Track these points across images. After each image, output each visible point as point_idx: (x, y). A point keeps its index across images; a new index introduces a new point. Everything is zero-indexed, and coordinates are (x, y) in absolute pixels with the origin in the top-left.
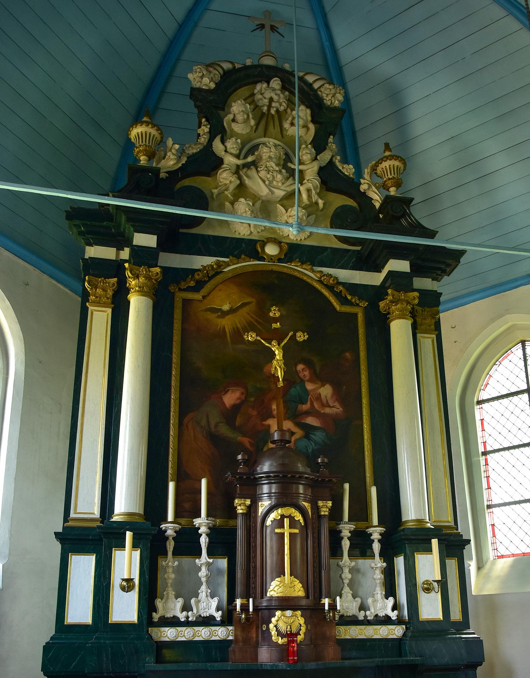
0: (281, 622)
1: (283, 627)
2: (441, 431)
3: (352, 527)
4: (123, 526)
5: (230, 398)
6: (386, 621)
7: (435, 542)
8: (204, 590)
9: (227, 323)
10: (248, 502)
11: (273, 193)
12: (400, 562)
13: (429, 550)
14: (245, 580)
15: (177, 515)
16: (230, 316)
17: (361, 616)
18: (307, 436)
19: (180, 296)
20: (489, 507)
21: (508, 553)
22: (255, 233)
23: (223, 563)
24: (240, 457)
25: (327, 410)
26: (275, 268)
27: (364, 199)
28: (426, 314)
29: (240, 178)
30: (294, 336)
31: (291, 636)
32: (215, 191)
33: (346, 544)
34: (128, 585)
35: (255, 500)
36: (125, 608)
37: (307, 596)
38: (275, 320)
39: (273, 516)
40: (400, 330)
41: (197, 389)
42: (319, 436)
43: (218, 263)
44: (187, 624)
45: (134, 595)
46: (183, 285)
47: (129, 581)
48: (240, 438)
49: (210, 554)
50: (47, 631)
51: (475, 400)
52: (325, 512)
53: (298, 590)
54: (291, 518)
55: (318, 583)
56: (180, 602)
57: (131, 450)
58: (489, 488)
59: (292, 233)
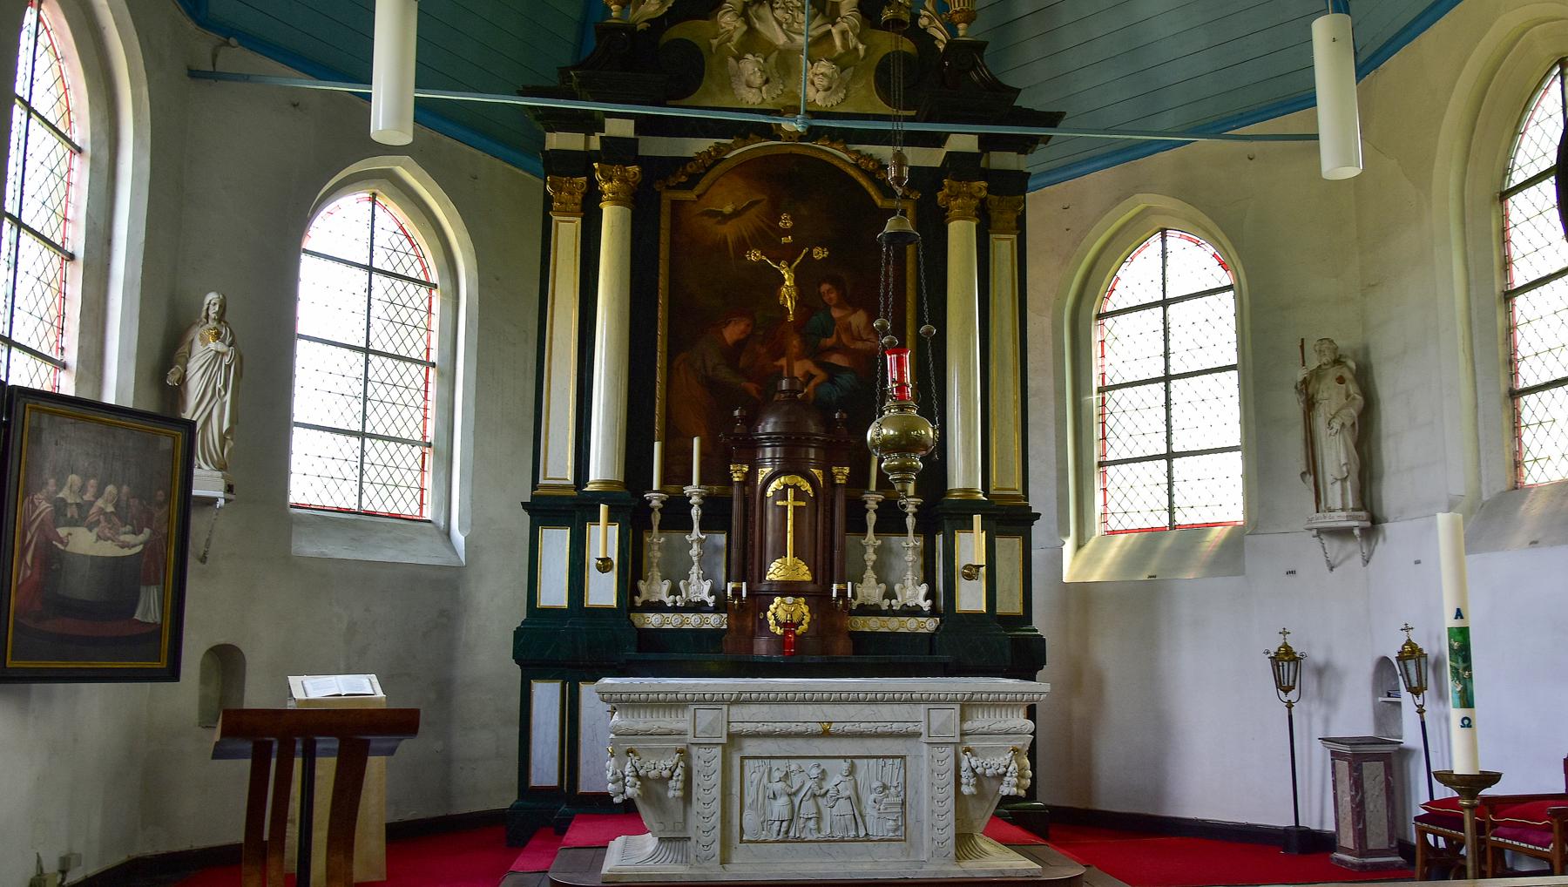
0: (779, 609)
1: (782, 615)
2: (1015, 369)
3: (880, 497)
4: (597, 497)
5: (732, 333)
6: (915, 612)
7: (977, 519)
8: (695, 571)
9: (729, 231)
10: (746, 469)
11: (791, 40)
12: (939, 539)
13: (971, 528)
14: (747, 563)
15: (665, 480)
16: (734, 222)
17: (885, 605)
18: (831, 380)
19: (667, 197)
20: (1101, 464)
21: (1120, 528)
22: (769, 100)
23: (721, 539)
24: (737, 413)
25: (859, 345)
26: (795, 150)
27: (923, 38)
28: (1002, 201)
29: (748, 22)
30: (810, 253)
31: (789, 626)
32: (715, 42)
33: (872, 518)
34: (605, 565)
35: (754, 467)
36: (603, 591)
37: (815, 580)
38: (786, 232)
39: (775, 485)
40: (960, 235)
41: (691, 323)
42: (846, 380)
43: (718, 147)
44: (675, 609)
45: (612, 577)
46: (672, 182)
47: (606, 560)
48: (745, 384)
49: (703, 529)
50: (519, 615)
51: (1094, 313)
52: (840, 480)
53: (804, 573)
54: (796, 488)
55: (829, 562)
56: (666, 586)
57: (607, 405)
58: (1104, 438)
59: (820, 99)
